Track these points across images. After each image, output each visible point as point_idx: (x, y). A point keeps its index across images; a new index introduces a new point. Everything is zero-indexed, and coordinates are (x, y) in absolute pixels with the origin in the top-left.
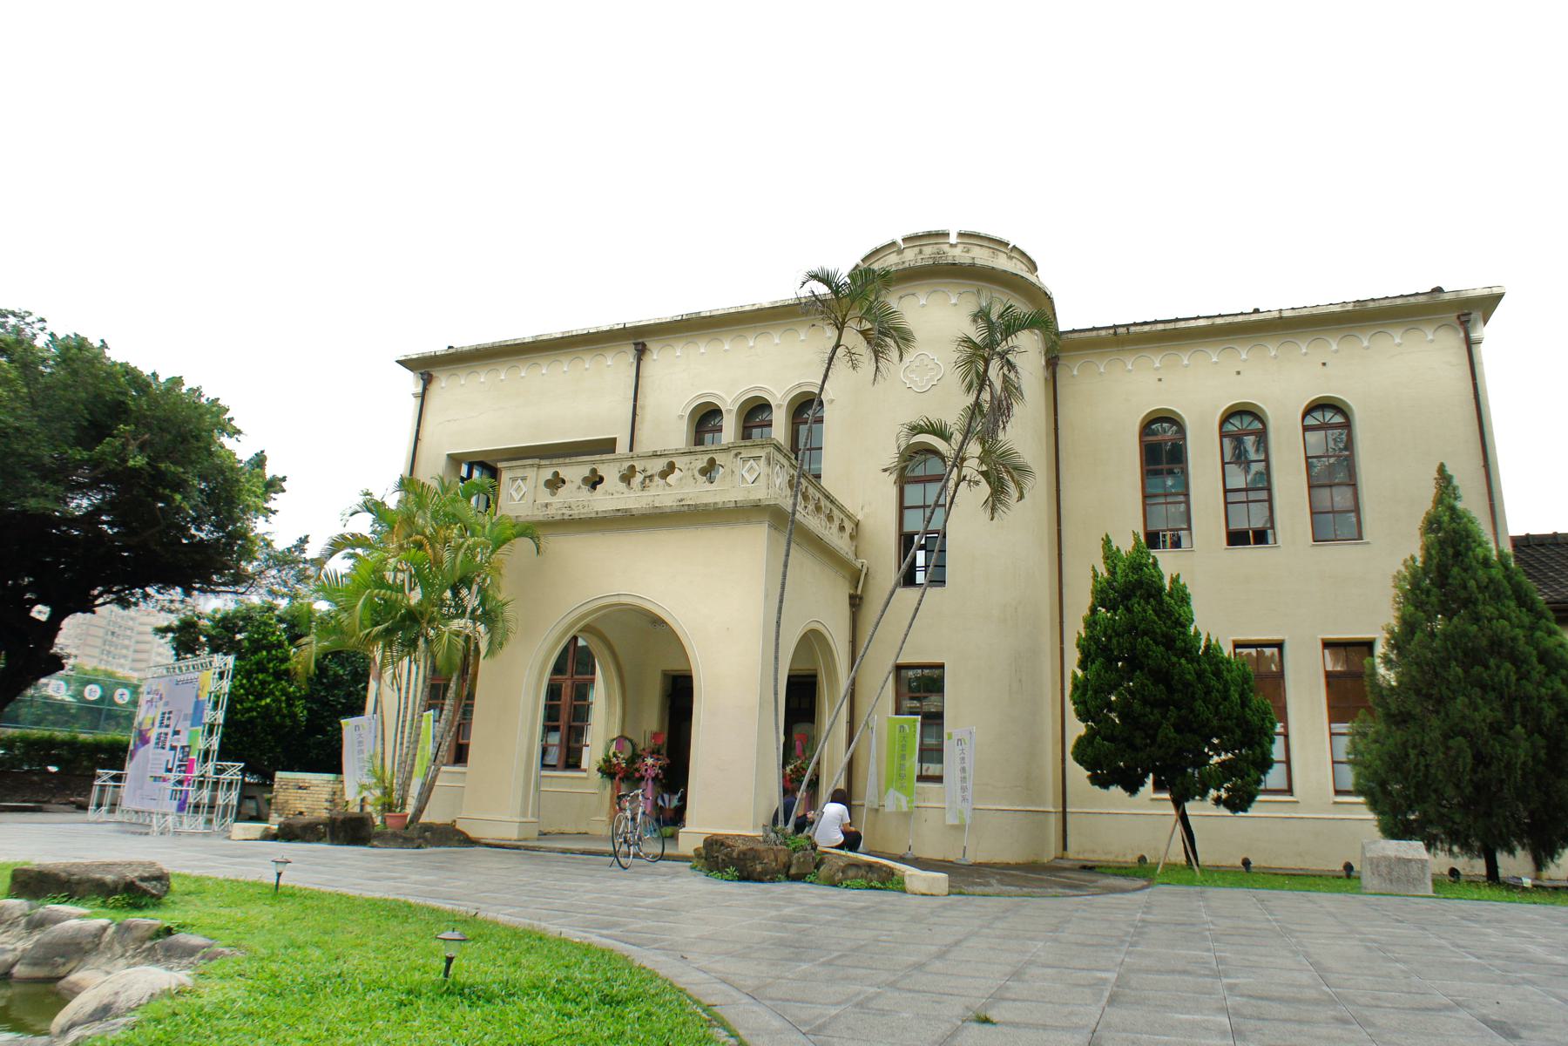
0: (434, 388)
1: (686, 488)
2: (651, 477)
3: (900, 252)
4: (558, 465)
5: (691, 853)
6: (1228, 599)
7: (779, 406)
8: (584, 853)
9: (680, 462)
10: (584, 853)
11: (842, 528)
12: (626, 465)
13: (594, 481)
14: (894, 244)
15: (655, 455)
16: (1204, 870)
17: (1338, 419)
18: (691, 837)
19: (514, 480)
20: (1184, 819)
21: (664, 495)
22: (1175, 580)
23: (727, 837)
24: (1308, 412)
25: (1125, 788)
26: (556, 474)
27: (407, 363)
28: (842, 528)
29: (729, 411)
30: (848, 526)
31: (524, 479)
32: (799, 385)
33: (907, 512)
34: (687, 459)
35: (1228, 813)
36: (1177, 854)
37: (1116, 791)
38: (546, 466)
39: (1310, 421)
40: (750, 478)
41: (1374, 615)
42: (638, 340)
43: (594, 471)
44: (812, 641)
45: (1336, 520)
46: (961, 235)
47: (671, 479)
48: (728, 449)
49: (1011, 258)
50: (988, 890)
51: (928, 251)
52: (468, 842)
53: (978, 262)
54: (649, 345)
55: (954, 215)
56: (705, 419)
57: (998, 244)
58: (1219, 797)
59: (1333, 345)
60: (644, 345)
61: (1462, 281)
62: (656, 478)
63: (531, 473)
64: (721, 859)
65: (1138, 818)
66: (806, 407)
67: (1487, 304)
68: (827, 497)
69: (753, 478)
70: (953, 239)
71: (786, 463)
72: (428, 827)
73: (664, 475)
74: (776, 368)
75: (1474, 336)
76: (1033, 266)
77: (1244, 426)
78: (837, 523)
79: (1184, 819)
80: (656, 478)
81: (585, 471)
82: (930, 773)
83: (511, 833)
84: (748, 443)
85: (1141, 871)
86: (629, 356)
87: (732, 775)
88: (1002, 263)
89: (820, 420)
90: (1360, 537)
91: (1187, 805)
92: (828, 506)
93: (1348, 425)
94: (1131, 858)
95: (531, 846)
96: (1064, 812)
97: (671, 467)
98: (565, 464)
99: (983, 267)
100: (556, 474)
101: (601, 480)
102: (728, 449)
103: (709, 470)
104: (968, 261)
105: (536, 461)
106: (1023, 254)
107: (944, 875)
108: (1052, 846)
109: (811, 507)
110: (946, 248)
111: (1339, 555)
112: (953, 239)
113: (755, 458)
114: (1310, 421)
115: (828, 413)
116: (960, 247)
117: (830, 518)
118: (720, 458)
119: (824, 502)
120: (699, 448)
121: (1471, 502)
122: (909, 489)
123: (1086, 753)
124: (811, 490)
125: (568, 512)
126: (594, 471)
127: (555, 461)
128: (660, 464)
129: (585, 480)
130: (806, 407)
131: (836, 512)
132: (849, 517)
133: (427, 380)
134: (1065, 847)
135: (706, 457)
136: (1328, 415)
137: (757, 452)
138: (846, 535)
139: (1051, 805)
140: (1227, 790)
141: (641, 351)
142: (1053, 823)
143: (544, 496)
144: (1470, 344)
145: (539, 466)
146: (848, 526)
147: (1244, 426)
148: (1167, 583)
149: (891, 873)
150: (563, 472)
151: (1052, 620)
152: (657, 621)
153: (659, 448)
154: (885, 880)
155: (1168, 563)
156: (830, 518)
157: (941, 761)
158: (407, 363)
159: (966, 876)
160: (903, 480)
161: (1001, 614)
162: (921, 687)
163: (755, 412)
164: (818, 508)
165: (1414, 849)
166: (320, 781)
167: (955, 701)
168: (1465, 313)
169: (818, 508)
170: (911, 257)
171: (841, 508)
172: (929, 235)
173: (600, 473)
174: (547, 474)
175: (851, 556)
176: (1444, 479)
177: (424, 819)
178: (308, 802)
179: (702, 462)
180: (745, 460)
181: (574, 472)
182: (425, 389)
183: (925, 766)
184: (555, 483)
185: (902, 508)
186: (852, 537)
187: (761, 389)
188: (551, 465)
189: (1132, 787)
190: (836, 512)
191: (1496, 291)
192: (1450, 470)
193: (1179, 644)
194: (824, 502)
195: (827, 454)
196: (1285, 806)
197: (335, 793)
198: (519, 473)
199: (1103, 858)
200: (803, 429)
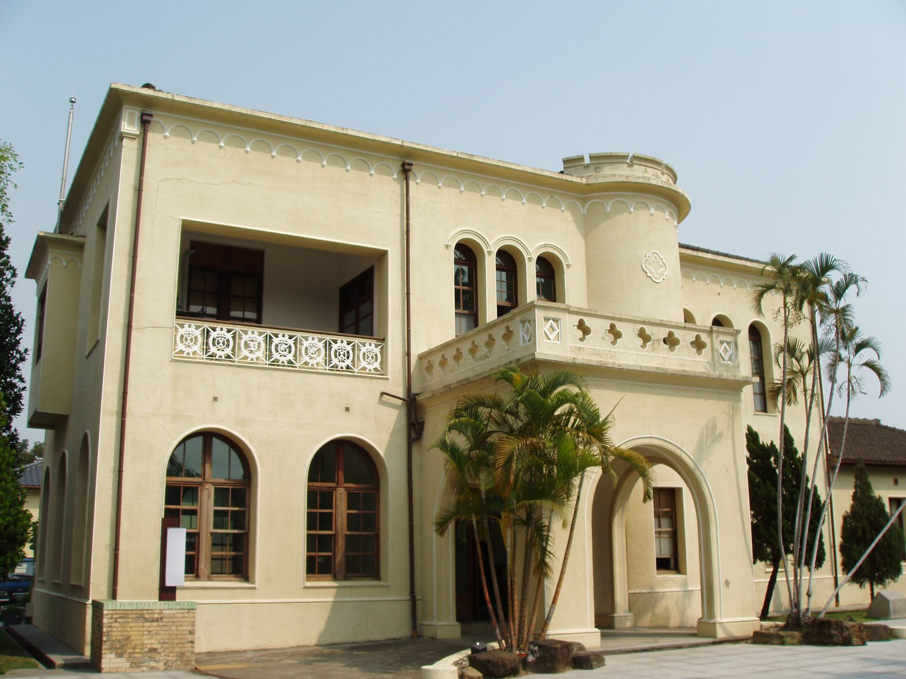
42: (406, 163)
170: (638, 174)
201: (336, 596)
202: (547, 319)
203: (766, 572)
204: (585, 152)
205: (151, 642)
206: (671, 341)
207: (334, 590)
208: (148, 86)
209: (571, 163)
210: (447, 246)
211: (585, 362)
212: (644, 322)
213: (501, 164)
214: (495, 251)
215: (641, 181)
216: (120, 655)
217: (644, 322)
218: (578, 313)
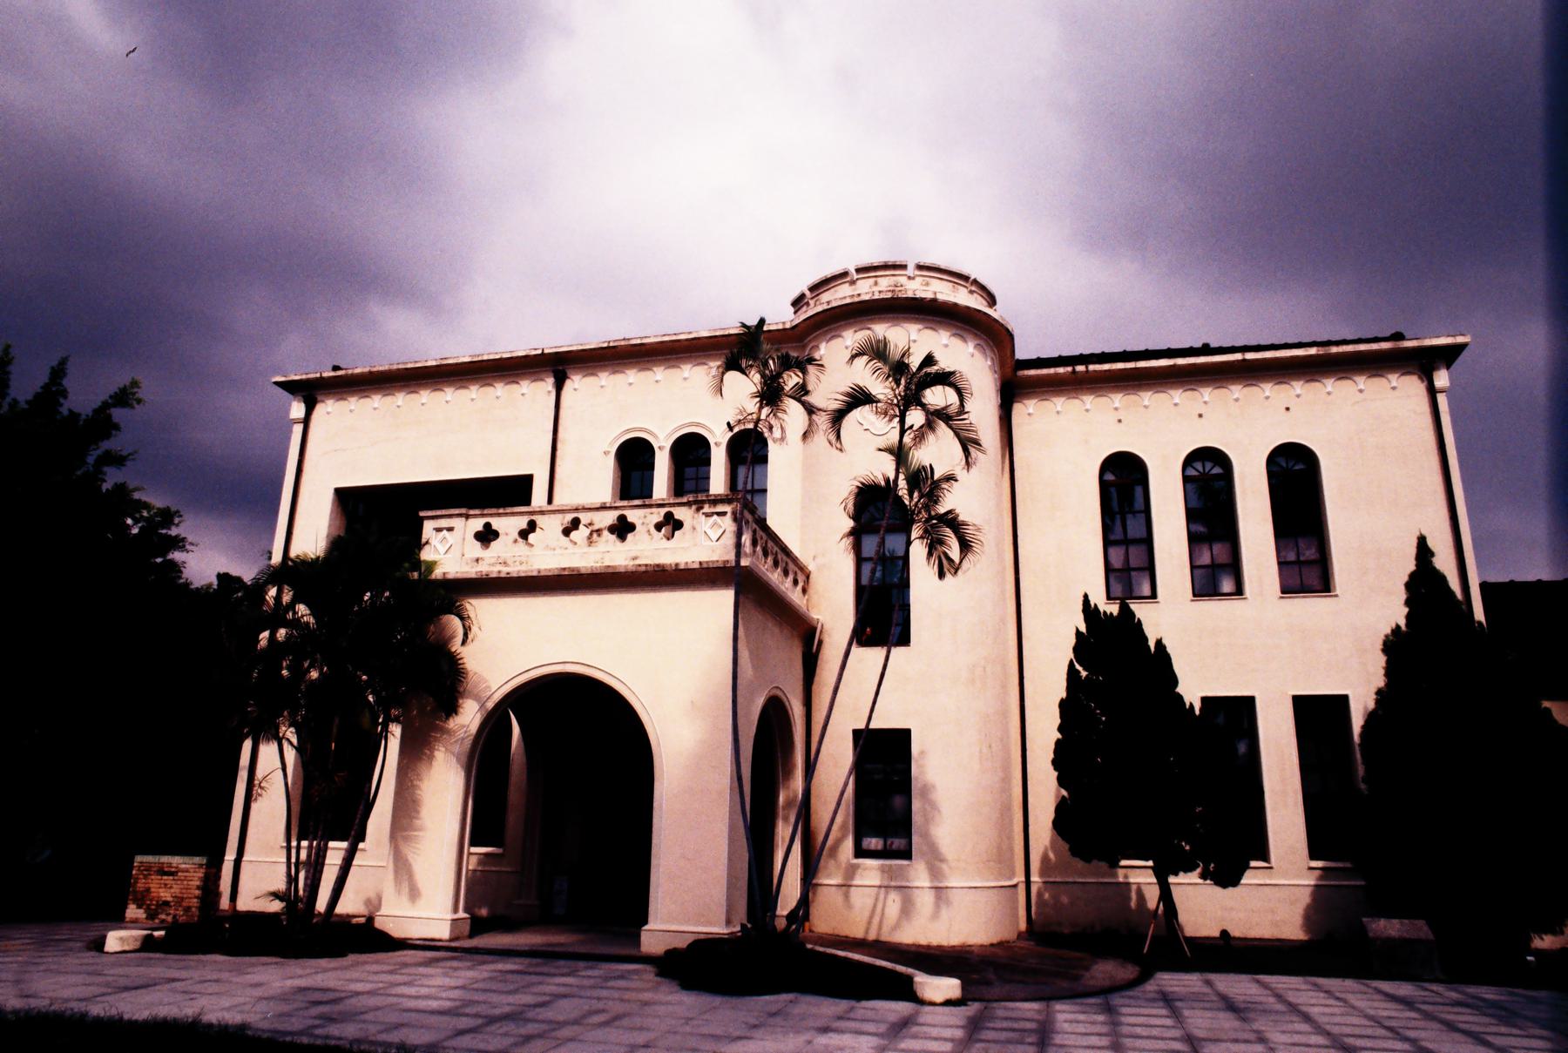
2: (599, 531)
3: (853, 282)
4: (491, 515)
8: (1088, 1047)
10: (1088, 1047)
14: (845, 274)
22: (1159, 643)
26: (488, 526)
30: (801, 578)
38: (475, 516)
40: (714, 536)
41: (1359, 682)
42: (558, 366)
45: (1307, 568)
49: (971, 292)
53: (941, 297)
56: (633, 459)
59: (1298, 390)
62: (606, 533)
63: (457, 523)
74: (711, 403)
76: (992, 300)
88: (963, 297)
98: (499, 515)
100: (488, 526)
104: (929, 295)
105: (463, 511)
106: (983, 288)
110: (903, 280)
111: (1308, 607)
116: (919, 280)
131: (791, 566)
138: (799, 587)
143: (475, 548)
145: (467, 517)
150: (496, 523)
163: (691, 450)
166: (189, 866)
169: (776, 564)
170: (866, 289)
171: (795, 560)
172: (886, 267)
173: (495, 526)
174: (477, 524)
176: (1424, 551)
177: (339, 909)
178: (176, 890)
181: (508, 524)
184: (487, 536)
188: (483, 515)
190: (791, 566)
198: (444, 523)
200: (742, 471)
201: (1320, 878)
202: (439, 530)
203: (1311, 868)
204: (802, 286)
205: (166, 895)
206: (622, 529)
207: (1318, 873)
208: (336, 368)
209: (798, 303)
210: (606, 453)
211: (460, 576)
212: (577, 510)
213: (666, 339)
214: (668, 445)
215: (848, 301)
216: (139, 907)
217: (577, 510)
218: (569, 511)
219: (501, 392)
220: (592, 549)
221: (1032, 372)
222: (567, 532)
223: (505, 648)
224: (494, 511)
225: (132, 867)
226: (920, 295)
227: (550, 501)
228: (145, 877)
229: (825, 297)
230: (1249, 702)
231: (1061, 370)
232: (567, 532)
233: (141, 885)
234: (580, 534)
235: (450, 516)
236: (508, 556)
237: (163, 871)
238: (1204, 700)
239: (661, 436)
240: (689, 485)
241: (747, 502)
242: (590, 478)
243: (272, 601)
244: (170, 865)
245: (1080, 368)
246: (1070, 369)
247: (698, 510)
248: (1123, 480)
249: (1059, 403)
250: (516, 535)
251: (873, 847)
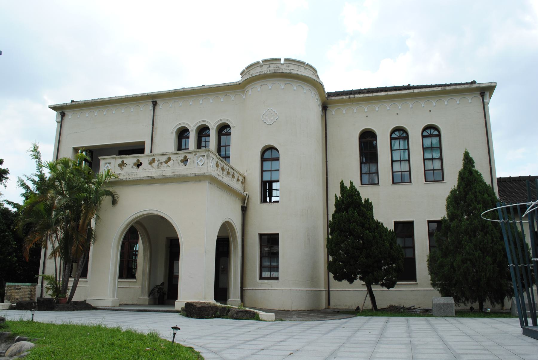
0: (66, 119)
1: (175, 168)
2: (161, 163)
3: (261, 66)
4: (124, 158)
5: (180, 309)
6: (388, 205)
7: (213, 129)
9: (172, 157)
11: (238, 180)
12: (151, 158)
13: (139, 165)
15: (163, 154)
16: (379, 310)
17: (436, 133)
18: (180, 304)
19: (106, 164)
20: (370, 292)
21: (167, 171)
23: (194, 303)
24: (425, 129)
25: (348, 281)
26: (123, 162)
27: (54, 108)
28: (238, 180)
29: (192, 130)
31: (110, 163)
32: (221, 120)
33: (264, 173)
34: (176, 156)
35: (386, 289)
36: (369, 304)
37: (345, 282)
39: (425, 133)
40: (200, 164)
42: (154, 100)
43: (138, 160)
44: (226, 227)
46: (286, 60)
47: (169, 163)
48: (192, 152)
49: (306, 69)
50: (292, 319)
51: (272, 67)
52: (95, 309)
54: (158, 102)
55: (283, 50)
56: (182, 134)
57: (300, 63)
58: (383, 283)
60: (156, 102)
61: (482, 80)
62: (163, 164)
63: (113, 161)
64: (193, 311)
65: (353, 292)
66: (224, 130)
67: (485, 91)
68: (232, 168)
69: (204, 163)
70: (282, 62)
71: (214, 157)
72: (76, 303)
73: (166, 162)
75: (485, 101)
76: (315, 71)
77: (400, 134)
78: (236, 178)
79: (370, 292)
80: (163, 164)
81: (135, 161)
82: (274, 276)
83: (109, 304)
84: (200, 150)
85: (356, 312)
86: (151, 106)
87: (195, 280)
88: (303, 72)
89: (230, 134)
90: (443, 180)
91: (372, 286)
92: (231, 172)
93: (439, 135)
94: (354, 308)
95: (120, 308)
96: (329, 291)
97: (169, 159)
98: (127, 158)
99: (294, 74)
100: (123, 162)
101: (141, 164)
102: (192, 152)
103: (185, 161)
105: (115, 156)
106: (311, 67)
107: (274, 314)
108: (324, 304)
109: (225, 173)
110: (279, 65)
112: (282, 62)
113: (202, 156)
114: (425, 133)
115: (233, 131)
116: (285, 65)
117: (233, 176)
118: (189, 156)
119: (230, 170)
120: (180, 152)
121: (480, 167)
122: (265, 163)
123: (331, 267)
124: (225, 166)
125: (128, 177)
126: (138, 160)
127: (122, 156)
128: (165, 158)
129: (135, 164)
130: (224, 130)
132: (241, 175)
133: (63, 115)
134: (329, 304)
135: (183, 156)
136: (432, 131)
137: (203, 154)
139: (323, 288)
140: (385, 280)
141: (155, 104)
142: (324, 295)
144: (484, 104)
145: (116, 158)
146: (241, 179)
147: (400, 134)
148: (363, 201)
149: (254, 314)
151: (324, 214)
152: (163, 218)
153: (164, 151)
154: (254, 316)
155: (366, 193)
156: (233, 176)
157: (277, 271)
158: (54, 108)
159: (282, 315)
160: (263, 160)
161: (298, 218)
162: (270, 242)
164: (228, 173)
165: (450, 300)
166: (25, 286)
167: (284, 249)
168: (485, 91)
169: (228, 173)
170: (265, 70)
171: (238, 172)
173: (141, 161)
174: (119, 161)
175: (242, 191)
178: (20, 295)
179: (181, 157)
180: (198, 157)
181: (130, 160)
182: (62, 119)
183: (272, 273)
185: (262, 171)
186: (242, 183)
187: (205, 121)
189: (351, 281)
190: (236, 174)
191: (493, 84)
192: (471, 155)
193: (367, 226)
194: (230, 170)
195: (232, 148)
196: (413, 286)
197: (31, 291)
198: (107, 161)
199: (344, 308)
200: (223, 138)
210: (172, 132)
215: (258, 74)
219: (132, 109)
220: (159, 170)
221: (334, 98)
222: (150, 163)
223: (134, 204)
224: (125, 156)
225: (5, 287)
226: (284, 71)
227: (151, 152)
228: (10, 290)
229: (252, 72)
230: (411, 223)
231: (344, 97)
232: (150, 163)
233: (8, 293)
234: (156, 164)
235: (110, 158)
236: (144, 172)
237: (16, 288)
238: (396, 224)
239: (192, 126)
240: (203, 144)
241: (222, 151)
242: (166, 142)
243: (15, 209)
244: (18, 286)
245: (352, 96)
246: (348, 97)
247: (195, 155)
248: (367, 140)
249: (464, 81)
250: (133, 165)
251: (266, 276)
